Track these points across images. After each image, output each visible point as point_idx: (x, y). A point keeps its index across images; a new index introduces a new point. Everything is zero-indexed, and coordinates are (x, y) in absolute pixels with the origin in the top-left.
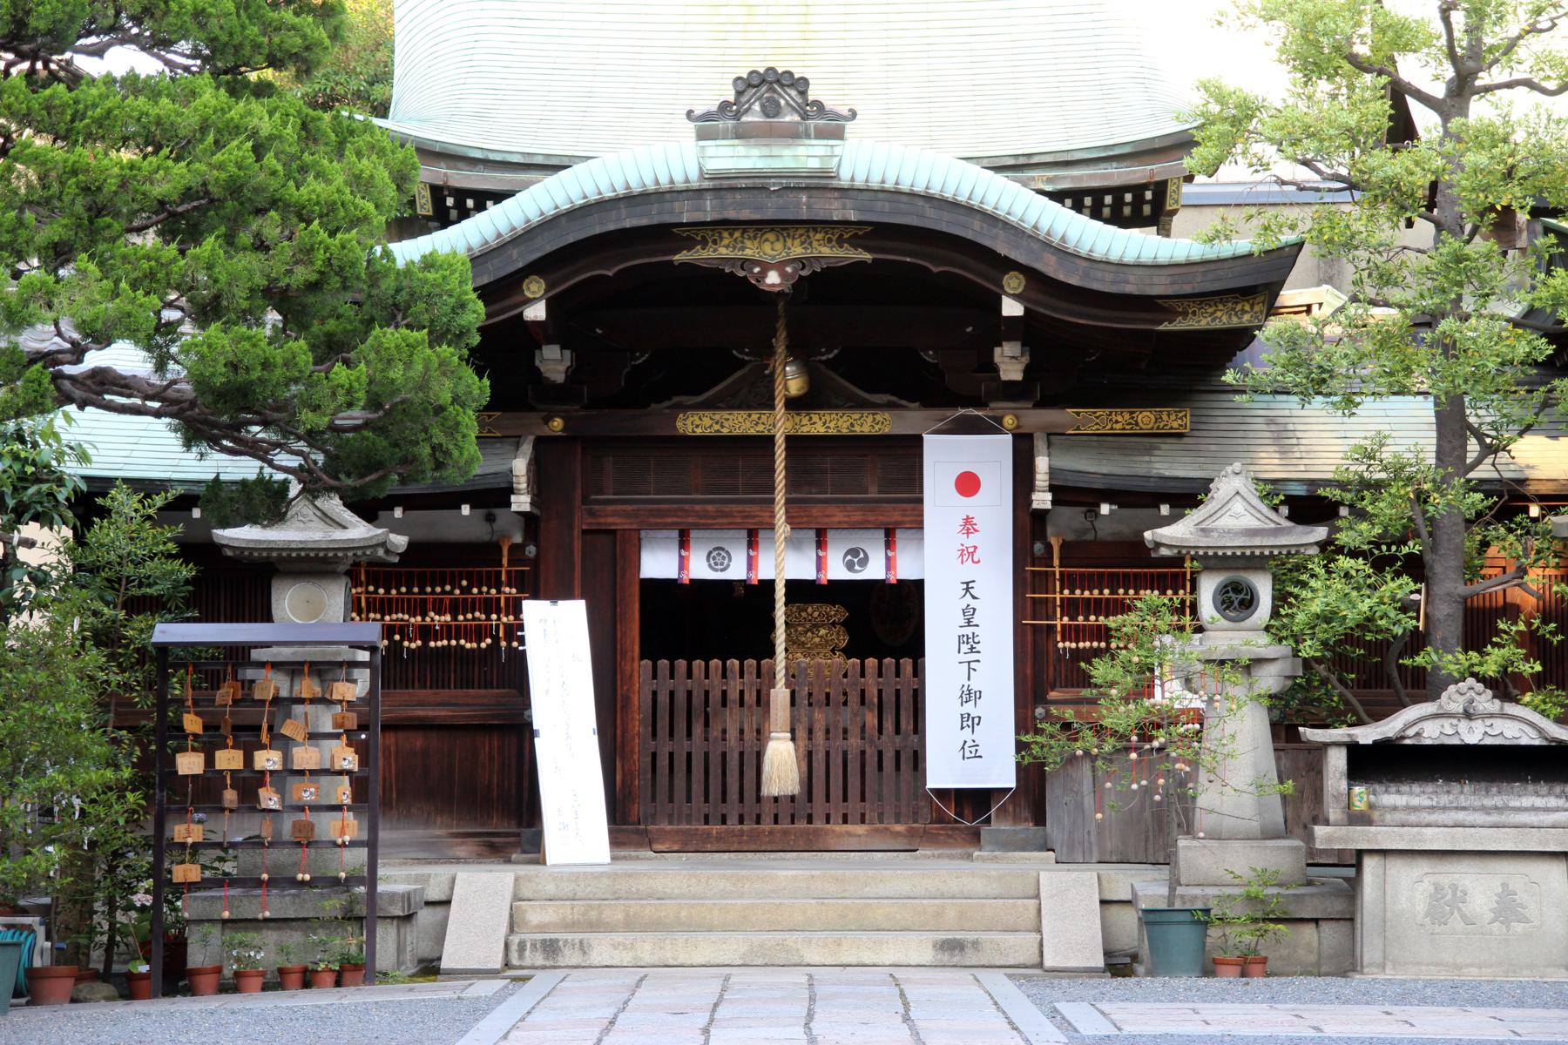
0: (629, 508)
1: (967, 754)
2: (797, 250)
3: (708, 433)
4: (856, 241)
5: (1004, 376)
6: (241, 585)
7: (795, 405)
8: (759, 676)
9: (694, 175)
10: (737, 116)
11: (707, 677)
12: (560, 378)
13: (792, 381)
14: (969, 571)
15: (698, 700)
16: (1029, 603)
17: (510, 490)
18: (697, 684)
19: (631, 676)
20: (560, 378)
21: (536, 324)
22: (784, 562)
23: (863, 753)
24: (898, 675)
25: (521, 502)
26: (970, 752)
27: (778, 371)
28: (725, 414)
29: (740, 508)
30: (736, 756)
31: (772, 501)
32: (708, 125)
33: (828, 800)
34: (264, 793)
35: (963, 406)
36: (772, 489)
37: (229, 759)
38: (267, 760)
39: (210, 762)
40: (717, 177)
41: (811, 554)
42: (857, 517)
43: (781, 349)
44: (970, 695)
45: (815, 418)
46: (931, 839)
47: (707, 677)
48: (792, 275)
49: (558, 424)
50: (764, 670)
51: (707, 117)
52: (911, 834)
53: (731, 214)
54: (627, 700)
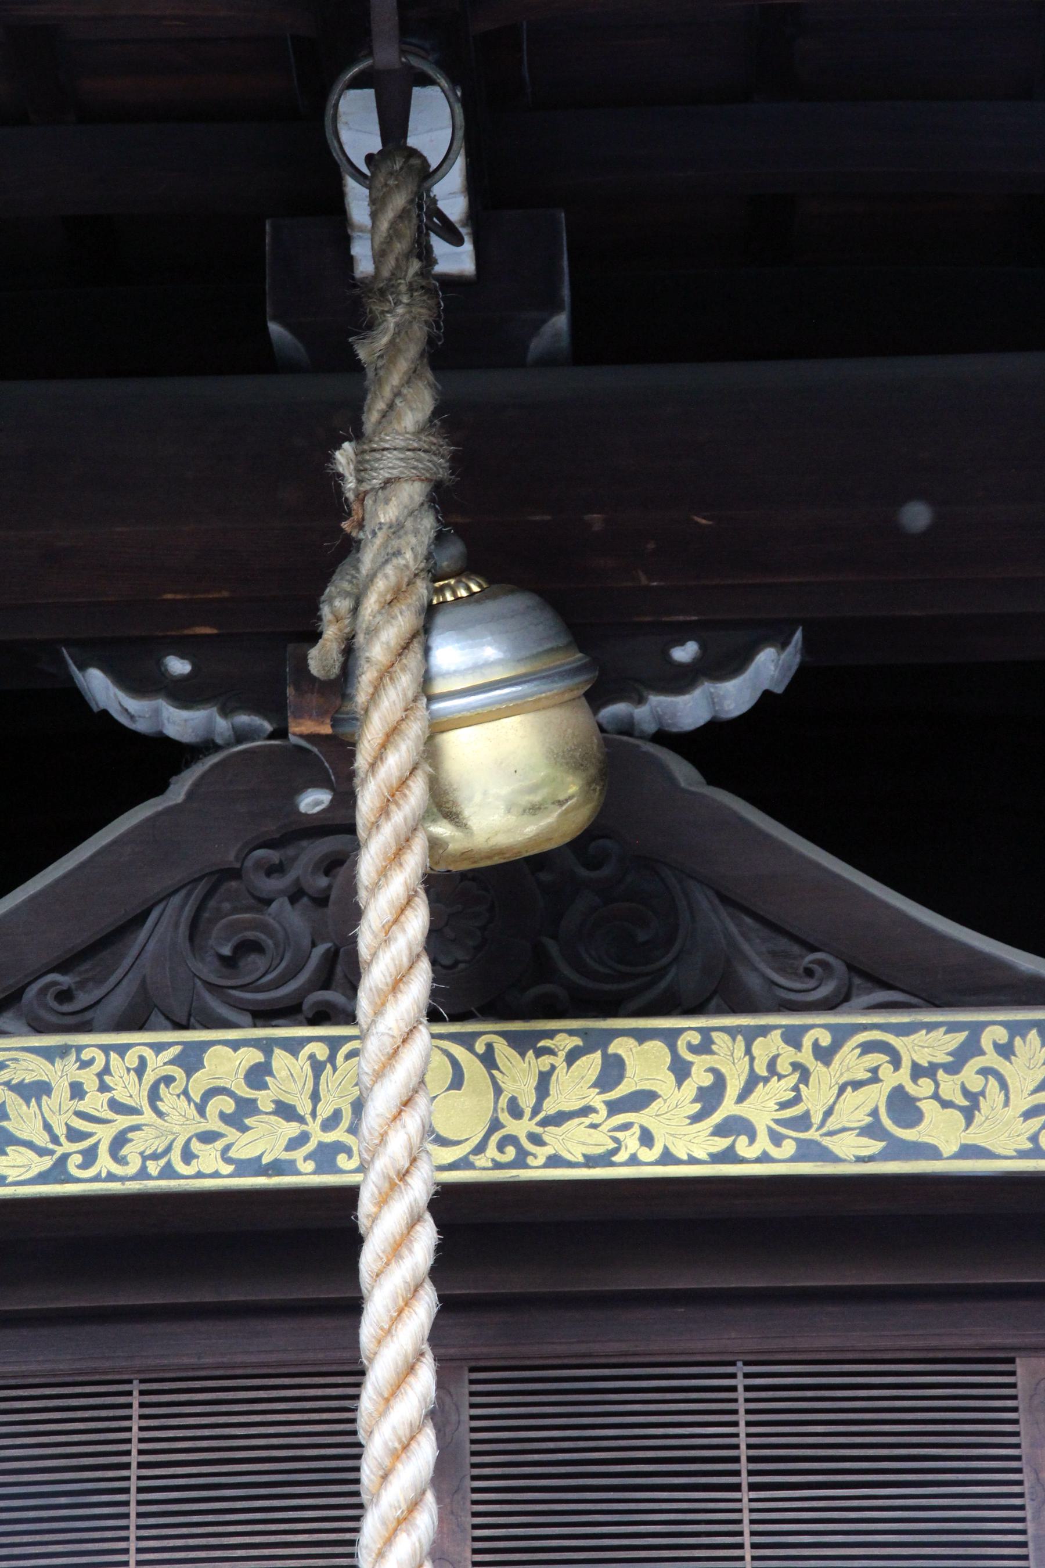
13: (470, 739)
27: (377, 651)
43: (391, 478)
45: (644, 1062)
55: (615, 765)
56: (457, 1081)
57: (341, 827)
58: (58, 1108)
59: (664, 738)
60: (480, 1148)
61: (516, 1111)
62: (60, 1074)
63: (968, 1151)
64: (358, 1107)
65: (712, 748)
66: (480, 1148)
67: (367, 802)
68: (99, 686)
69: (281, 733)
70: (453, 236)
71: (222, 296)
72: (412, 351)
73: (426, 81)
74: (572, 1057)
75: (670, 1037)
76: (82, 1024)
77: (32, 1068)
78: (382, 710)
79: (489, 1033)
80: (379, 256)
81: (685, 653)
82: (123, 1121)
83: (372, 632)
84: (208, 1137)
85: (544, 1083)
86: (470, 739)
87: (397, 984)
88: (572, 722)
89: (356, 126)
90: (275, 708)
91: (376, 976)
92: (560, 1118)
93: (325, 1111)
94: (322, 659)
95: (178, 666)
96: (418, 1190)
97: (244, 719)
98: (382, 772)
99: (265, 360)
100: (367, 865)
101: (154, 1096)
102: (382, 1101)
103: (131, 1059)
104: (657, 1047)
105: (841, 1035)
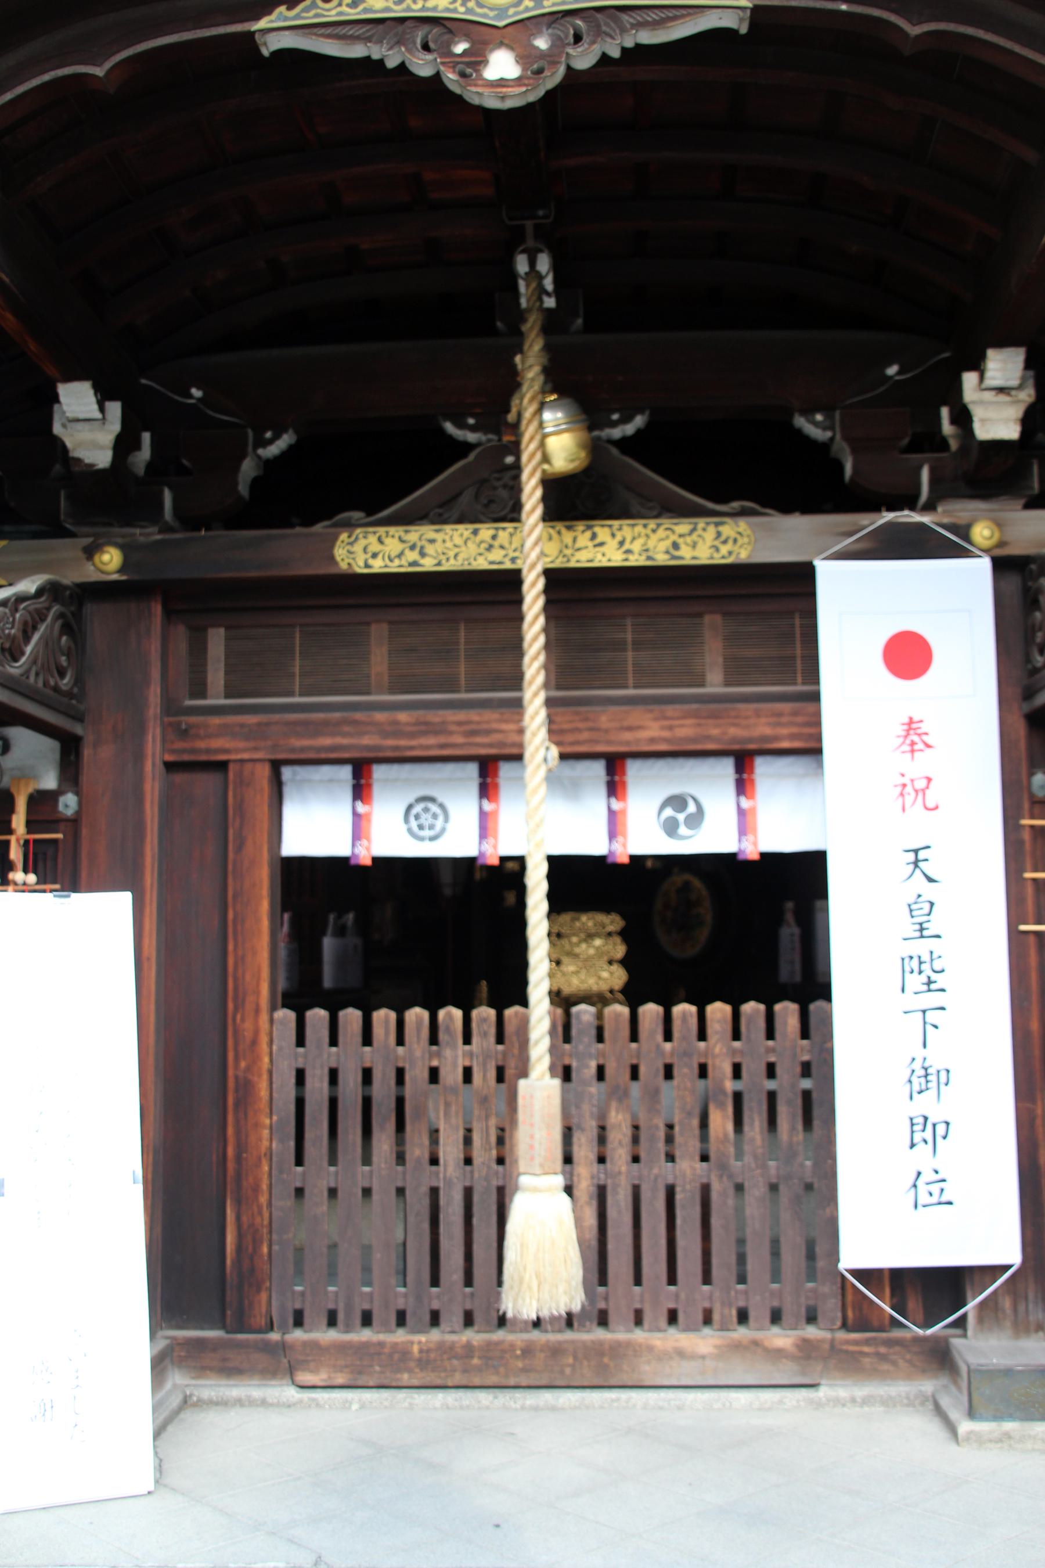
0: (251, 719)
1: (924, 1198)
3: (394, 568)
5: (983, 432)
8: (500, 1039)
11: (400, 1041)
13: (553, 440)
14: (917, 827)
15: (383, 1089)
16: (1030, 890)
18: (382, 1054)
19: (255, 1042)
20: (102, 458)
22: (545, 818)
23: (705, 1190)
24: (770, 1034)
26: (931, 1193)
27: (527, 414)
28: (428, 531)
29: (461, 715)
30: (458, 1197)
31: (518, 705)
33: (638, 1281)
35: (891, 509)
36: (516, 680)
41: (595, 805)
42: (686, 730)
43: (531, 365)
44: (927, 1078)
45: (602, 532)
46: (846, 1363)
47: (400, 1041)
48: (550, 58)
49: (111, 559)
50: (510, 1028)
52: (807, 1351)
54: (246, 1088)
55: (595, 449)
56: (550, 538)
57: (517, 467)
58: (439, 546)
59: (611, 442)
60: (557, 558)
61: (566, 547)
62: (439, 537)
63: (694, 558)
64: (522, 546)
65: (624, 444)
66: (557, 558)
67: (524, 458)
68: (449, 427)
69: (500, 440)
70: (548, 294)
71: (484, 316)
72: (537, 328)
73: (541, 251)
74: (583, 532)
75: (610, 526)
76: (445, 522)
77: (432, 535)
78: (529, 431)
79: (560, 526)
80: (528, 301)
81: (615, 417)
82: (457, 550)
83: (526, 409)
84: (480, 554)
85: (575, 540)
86: (553, 440)
87: (533, 510)
88: (583, 435)
89: (522, 265)
90: (498, 432)
91: (527, 507)
92: (579, 549)
93: (514, 546)
94: (511, 417)
95: (471, 421)
96: (539, 568)
97: (490, 436)
98: (529, 449)
99: (493, 332)
100: (524, 476)
101: (466, 543)
102: (529, 543)
103: (459, 532)
104: (607, 530)
105: (659, 525)
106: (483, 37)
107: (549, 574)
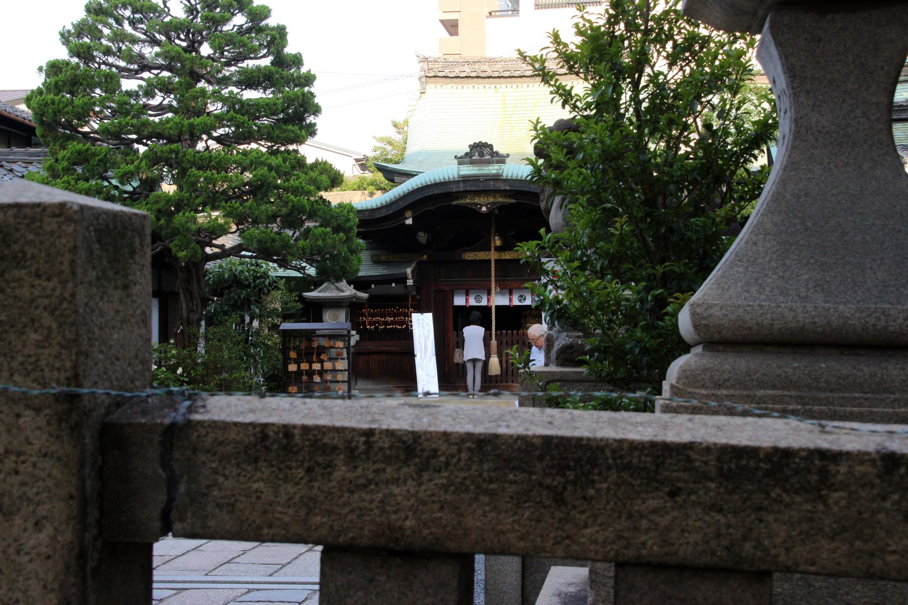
2: (491, 200)
4: (510, 197)
6: (314, 310)
7: (498, 249)
9: (456, 176)
10: (471, 157)
12: (424, 242)
17: (407, 278)
20: (424, 242)
21: (409, 225)
25: (410, 282)
32: (462, 160)
34: (315, 377)
37: (305, 366)
38: (317, 366)
39: (299, 367)
40: (463, 176)
43: (493, 232)
49: (425, 257)
51: (461, 157)
53: (469, 188)
106: (482, 206)
107: (496, 260)
